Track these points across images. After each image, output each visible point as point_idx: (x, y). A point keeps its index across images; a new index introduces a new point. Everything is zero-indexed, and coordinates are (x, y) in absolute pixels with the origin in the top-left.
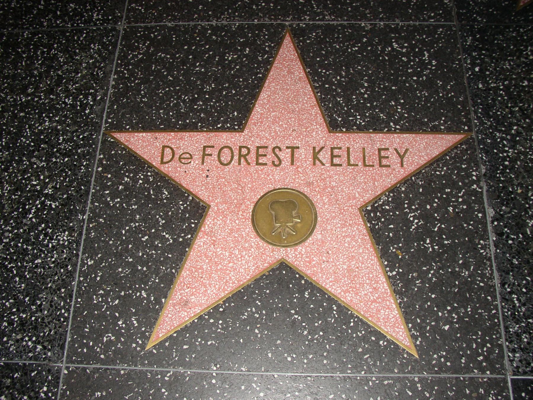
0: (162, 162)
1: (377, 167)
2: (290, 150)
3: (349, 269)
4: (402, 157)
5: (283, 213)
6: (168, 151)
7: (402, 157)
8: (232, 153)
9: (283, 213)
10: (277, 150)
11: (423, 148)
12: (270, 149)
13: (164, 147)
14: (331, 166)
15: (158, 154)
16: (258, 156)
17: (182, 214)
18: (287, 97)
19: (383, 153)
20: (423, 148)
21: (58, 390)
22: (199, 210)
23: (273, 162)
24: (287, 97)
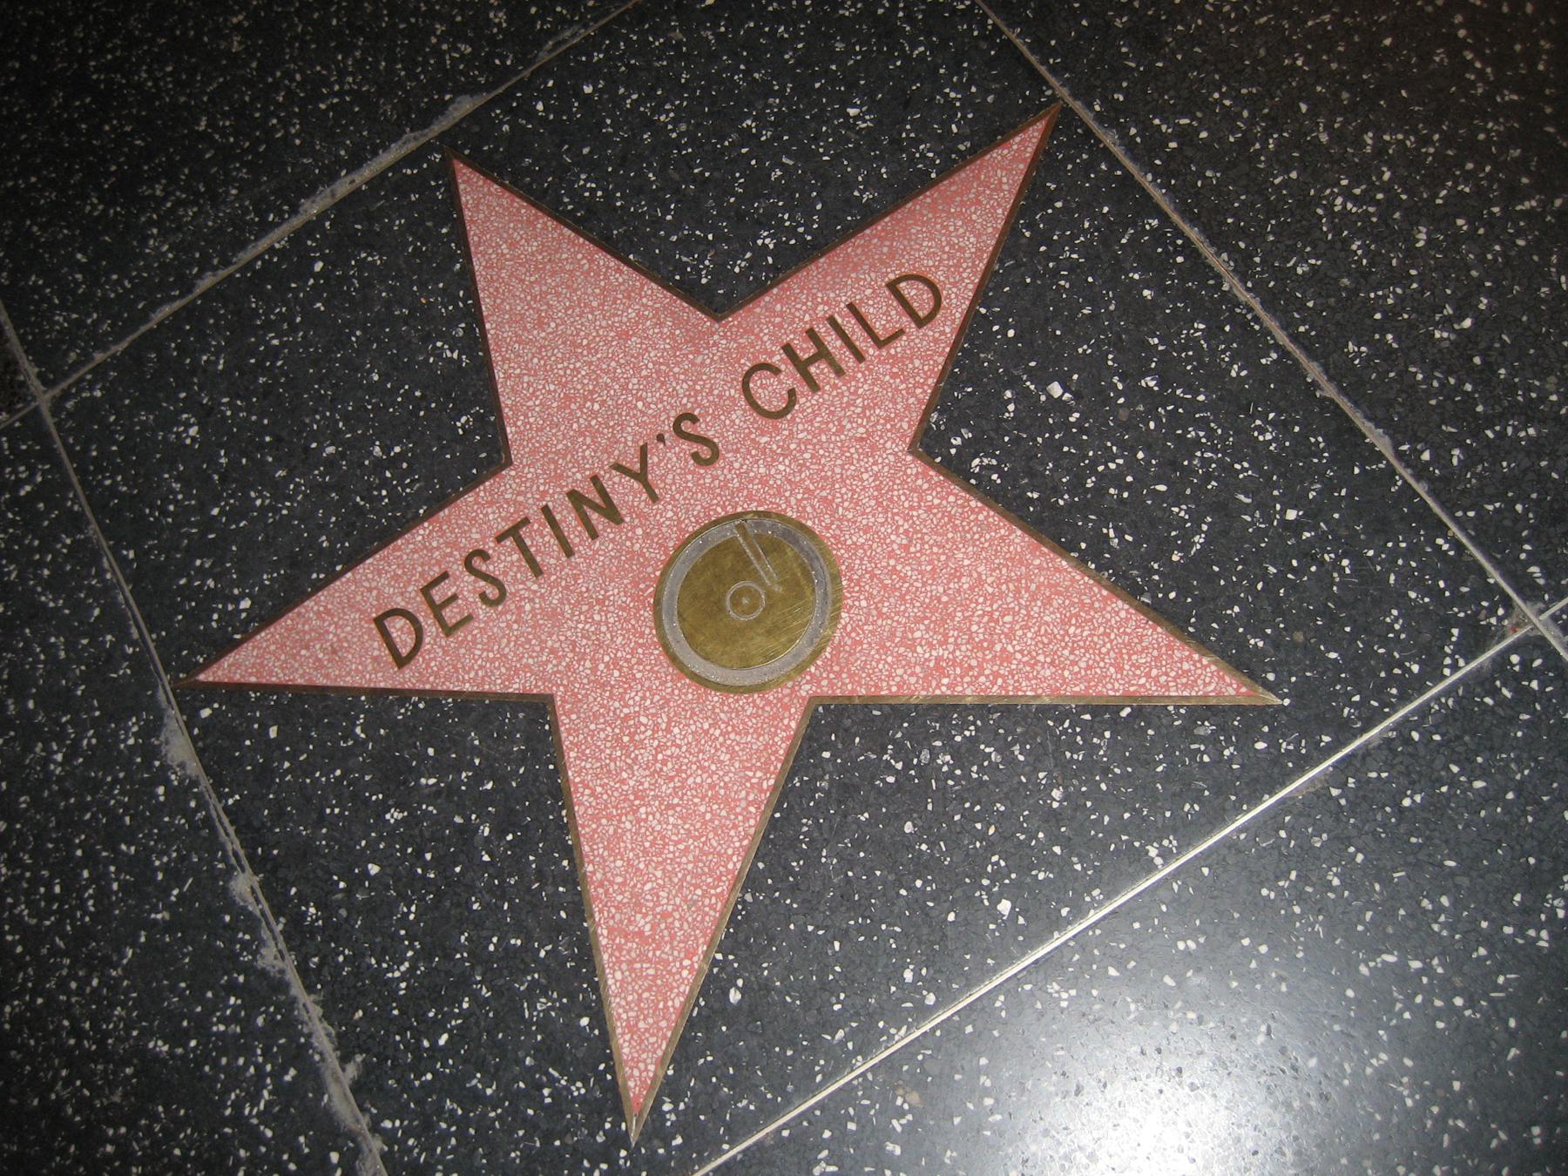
0: (401, 661)
1: (911, 328)
2: (508, 542)
3: (983, 611)
4: (641, 476)
5: (743, 585)
6: (908, 290)
7: (641, 476)
8: (413, 619)
9: (743, 585)
10: (477, 562)
11: (953, 235)
12: (458, 568)
13: (379, 622)
14: (447, 635)
15: (377, 647)
16: (437, 610)
17: (515, 743)
18: (569, 329)
19: (438, 595)
20: (953, 235)
21: (1402, 477)
22: (536, 713)
23: (483, 596)
24: (569, 329)
